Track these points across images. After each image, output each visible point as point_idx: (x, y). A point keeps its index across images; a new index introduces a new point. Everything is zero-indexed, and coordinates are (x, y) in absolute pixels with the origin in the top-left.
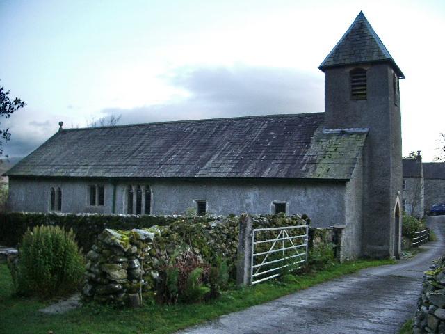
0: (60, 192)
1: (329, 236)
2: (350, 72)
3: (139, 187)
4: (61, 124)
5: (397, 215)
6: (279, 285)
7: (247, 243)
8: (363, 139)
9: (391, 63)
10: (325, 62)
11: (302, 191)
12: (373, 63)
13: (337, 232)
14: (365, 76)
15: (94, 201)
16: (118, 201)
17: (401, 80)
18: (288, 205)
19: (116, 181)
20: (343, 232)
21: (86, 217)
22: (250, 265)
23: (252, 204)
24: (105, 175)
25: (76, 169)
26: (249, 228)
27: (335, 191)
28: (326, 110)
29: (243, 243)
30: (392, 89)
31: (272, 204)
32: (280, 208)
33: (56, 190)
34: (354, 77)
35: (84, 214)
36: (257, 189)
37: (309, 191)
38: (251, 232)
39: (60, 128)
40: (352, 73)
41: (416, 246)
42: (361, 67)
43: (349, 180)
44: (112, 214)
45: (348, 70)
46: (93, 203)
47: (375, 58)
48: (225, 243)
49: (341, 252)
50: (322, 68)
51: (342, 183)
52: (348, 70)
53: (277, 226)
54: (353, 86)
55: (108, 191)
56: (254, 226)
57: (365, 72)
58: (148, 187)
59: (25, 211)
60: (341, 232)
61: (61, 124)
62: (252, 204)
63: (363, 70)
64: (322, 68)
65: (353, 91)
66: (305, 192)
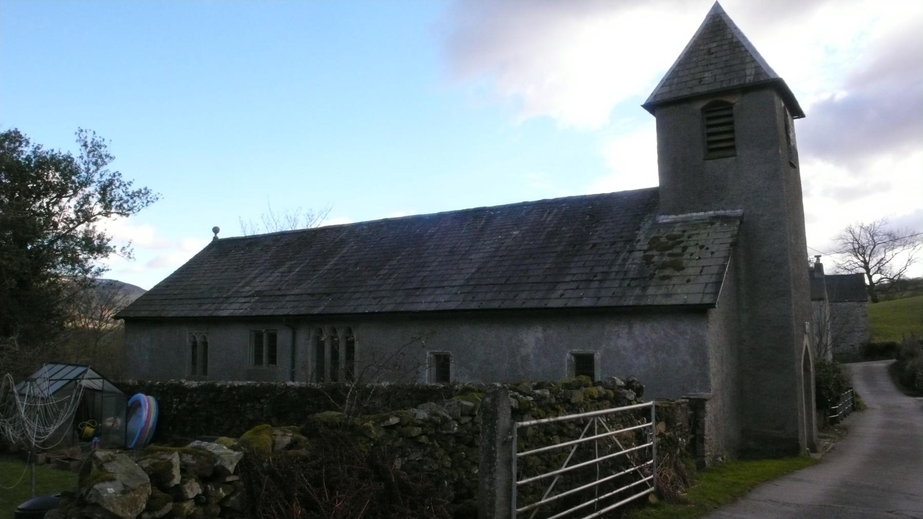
0: (205, 344)
1: (681, 418)
2: (702, 109)
3: (335, 331)
4: (216, 230)
5: (807, 370)
6: (612, 389)
7: (499, 456)
8: (734, 228)
9: (779, 88)
10: (655, 95)
11: (623, 330)
12: (745, 89)
13: (697, 406)
14: (731, 115)
15: (261, 357)
16: (299, 357)
17: (797, 122)
18: (597, 357)
19: (294, 322)
20: (708, 406)
21: (232, 388)
22: (510, 509)
23: (532, 356)
24: (277, 313)
25: (200, 305)
26: (504, 419)
27: (687, 327)
28: (663, 173)
29: (491, 458)
30: (785, 141)
31: (568, 355)
32: (584, 364)
33: (198, 339)
34: (709, 119)
35: (230, 382)
36: (540, 329)
37: (637, 328)
38: (510, 430)
39: (215, 238)
40: (705, 110)
41: (835, 421)
42: (719, 99)
43: (712, 306)
44: (290, 383)
45: (700, 105)
46: (258, 359)
47: (749, 79)
48: (451, 455)
49: (707, 447)
50: (651, 107)
51: (699, 311)
52: (700, 105)
53: (574, 409)
54: (709, 135)
55: (284, 337)
56: (518, 414)
57: (730, 106)
58: (350, 331)
59: (188, 379)
60: (703, 408)
61: (216, 230)
62: (532, 356)
63: (727, 103)
64: (651, 107)
65: (710, 143)
66: (631, 327)
